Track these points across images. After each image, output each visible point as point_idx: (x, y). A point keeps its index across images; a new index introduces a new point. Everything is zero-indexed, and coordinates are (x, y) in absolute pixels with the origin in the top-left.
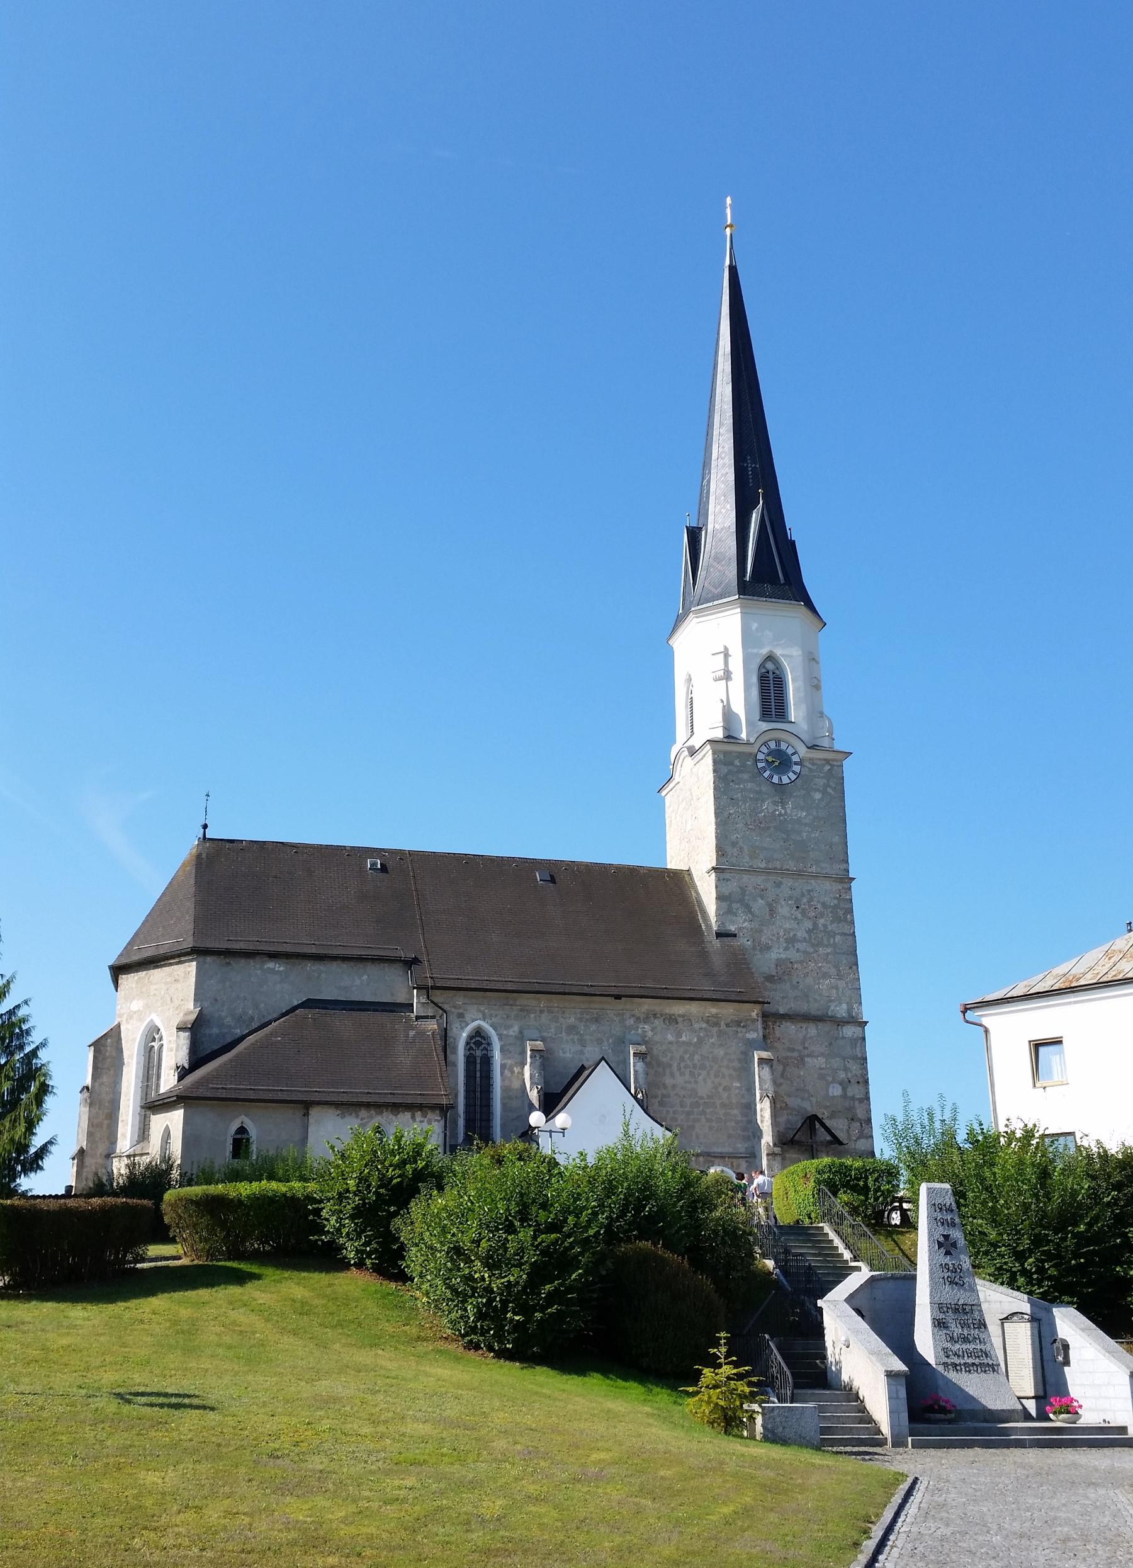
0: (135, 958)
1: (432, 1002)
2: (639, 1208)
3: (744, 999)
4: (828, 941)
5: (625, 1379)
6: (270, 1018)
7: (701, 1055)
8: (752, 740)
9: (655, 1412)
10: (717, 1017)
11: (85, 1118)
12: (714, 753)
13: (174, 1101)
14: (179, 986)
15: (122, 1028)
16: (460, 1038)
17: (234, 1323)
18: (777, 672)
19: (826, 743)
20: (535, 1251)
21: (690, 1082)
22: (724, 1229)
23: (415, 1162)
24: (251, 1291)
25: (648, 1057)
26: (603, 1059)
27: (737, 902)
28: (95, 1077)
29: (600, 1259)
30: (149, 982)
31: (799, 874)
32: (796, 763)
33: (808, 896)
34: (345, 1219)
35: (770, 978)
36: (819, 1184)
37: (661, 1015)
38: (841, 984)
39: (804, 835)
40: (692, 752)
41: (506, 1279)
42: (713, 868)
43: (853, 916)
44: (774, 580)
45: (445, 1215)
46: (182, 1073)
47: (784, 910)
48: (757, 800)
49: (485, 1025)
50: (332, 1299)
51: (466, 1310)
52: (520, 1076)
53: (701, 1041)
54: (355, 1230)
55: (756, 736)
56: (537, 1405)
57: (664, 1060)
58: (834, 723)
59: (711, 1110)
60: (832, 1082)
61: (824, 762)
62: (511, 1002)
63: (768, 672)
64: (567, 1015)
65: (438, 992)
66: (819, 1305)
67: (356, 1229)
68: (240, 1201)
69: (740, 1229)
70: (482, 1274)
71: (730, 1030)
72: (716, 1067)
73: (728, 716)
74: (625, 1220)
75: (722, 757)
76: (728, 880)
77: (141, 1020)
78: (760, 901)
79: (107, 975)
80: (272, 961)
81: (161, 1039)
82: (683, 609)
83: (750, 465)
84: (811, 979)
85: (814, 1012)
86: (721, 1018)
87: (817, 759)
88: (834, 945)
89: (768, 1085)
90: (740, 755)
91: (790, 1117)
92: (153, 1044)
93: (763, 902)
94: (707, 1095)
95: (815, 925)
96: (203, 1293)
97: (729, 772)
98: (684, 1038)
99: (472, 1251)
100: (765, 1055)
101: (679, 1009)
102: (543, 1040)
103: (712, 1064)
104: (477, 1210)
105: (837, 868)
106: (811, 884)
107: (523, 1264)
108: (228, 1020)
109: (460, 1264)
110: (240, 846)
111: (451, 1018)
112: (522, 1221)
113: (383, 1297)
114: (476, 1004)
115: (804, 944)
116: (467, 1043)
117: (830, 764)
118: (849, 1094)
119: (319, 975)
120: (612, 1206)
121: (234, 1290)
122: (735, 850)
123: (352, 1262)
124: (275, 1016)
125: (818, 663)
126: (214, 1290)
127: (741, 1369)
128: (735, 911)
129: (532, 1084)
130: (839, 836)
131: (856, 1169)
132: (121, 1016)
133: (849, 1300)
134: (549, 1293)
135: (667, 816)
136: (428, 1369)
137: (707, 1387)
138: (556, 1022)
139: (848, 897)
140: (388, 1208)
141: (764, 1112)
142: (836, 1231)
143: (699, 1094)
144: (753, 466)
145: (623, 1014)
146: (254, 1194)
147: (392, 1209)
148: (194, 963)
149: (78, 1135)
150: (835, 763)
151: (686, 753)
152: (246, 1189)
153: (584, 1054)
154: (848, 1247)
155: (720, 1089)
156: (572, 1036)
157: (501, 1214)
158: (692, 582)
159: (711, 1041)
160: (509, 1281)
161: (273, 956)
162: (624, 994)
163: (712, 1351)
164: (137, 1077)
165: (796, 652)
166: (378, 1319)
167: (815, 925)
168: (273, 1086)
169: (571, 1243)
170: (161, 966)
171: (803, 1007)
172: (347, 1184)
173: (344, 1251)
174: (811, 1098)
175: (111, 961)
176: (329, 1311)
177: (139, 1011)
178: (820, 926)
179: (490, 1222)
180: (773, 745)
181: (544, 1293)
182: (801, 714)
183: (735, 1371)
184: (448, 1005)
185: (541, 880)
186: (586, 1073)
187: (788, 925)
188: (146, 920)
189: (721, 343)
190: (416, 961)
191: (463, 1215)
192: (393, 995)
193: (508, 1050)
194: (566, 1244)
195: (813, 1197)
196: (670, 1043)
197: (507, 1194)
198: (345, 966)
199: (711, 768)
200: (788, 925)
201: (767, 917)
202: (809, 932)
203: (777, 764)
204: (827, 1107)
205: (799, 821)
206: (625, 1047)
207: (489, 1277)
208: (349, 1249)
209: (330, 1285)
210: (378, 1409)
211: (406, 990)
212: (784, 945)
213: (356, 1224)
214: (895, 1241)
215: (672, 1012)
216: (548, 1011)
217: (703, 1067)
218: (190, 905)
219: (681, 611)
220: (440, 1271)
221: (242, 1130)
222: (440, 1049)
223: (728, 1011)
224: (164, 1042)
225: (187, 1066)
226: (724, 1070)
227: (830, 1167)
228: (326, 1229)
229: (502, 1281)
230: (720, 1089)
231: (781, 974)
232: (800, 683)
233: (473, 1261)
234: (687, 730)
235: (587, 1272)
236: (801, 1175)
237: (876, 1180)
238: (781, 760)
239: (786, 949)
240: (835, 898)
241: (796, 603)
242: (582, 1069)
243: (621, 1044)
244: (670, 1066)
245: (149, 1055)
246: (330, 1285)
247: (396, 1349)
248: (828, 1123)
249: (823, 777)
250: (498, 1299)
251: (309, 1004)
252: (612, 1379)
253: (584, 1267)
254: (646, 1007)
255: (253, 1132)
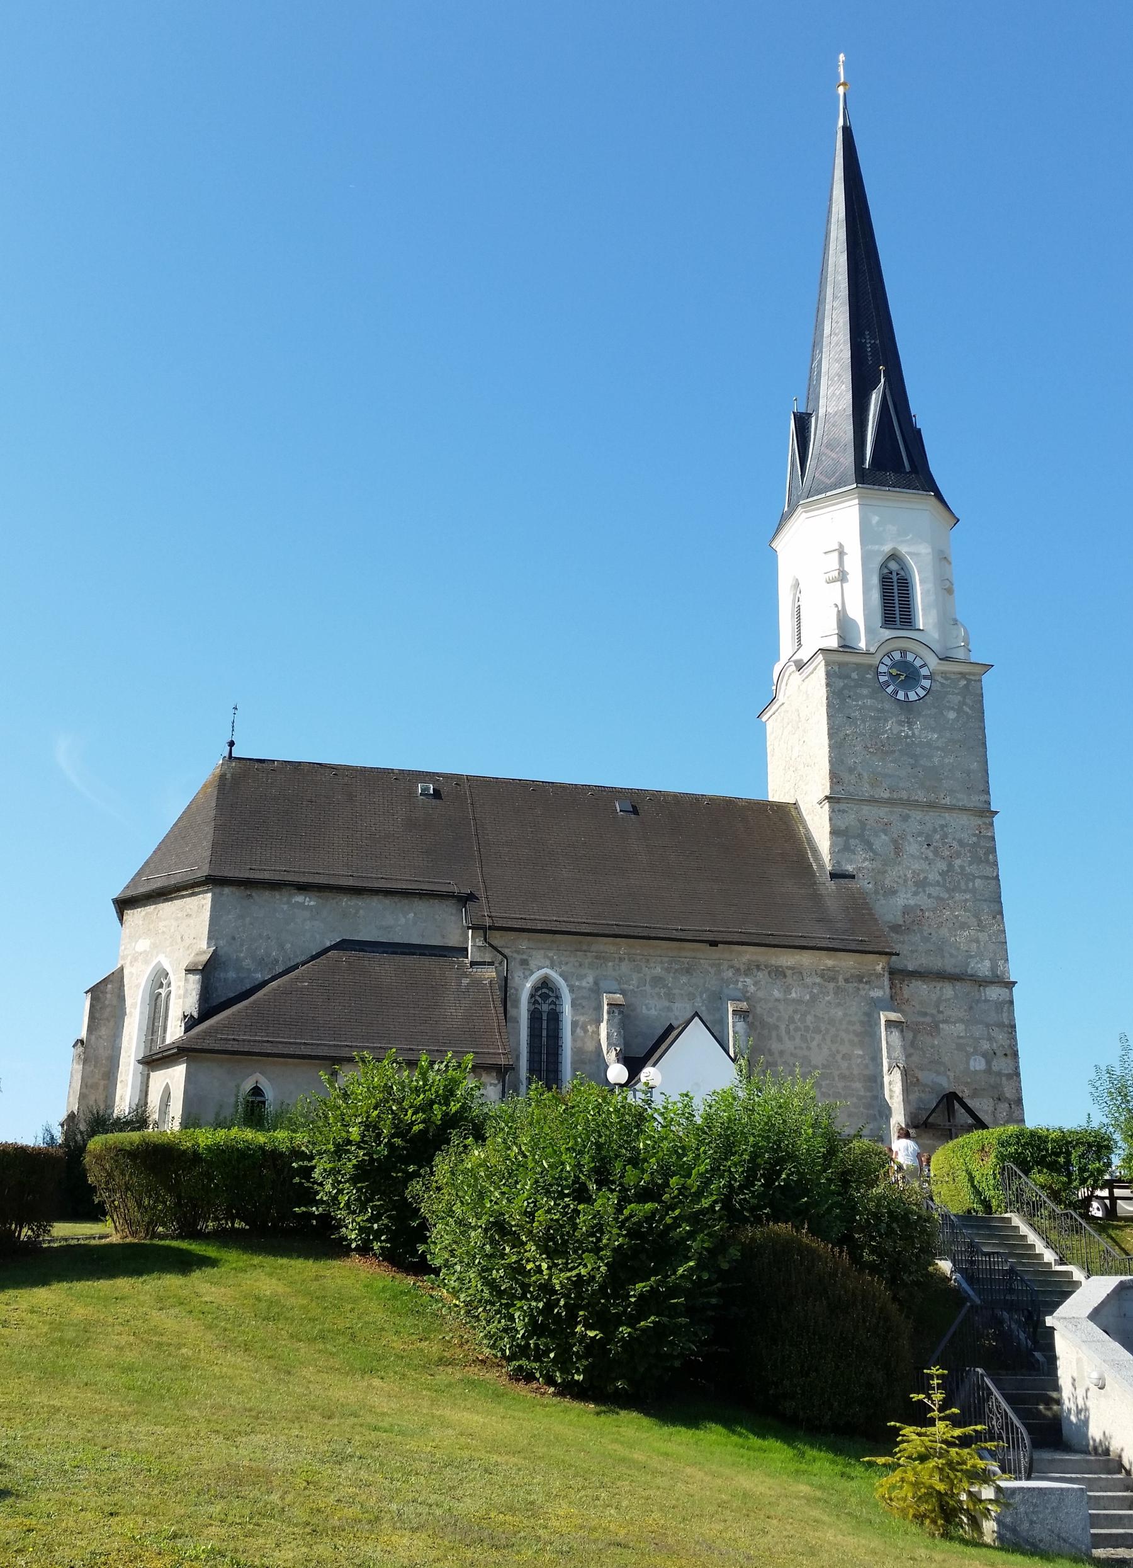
0: (142, 890)
1: (491, 945)
2: (772, 1175)
3: (867, 949)
4: (967, 884)
5: (762, 1435)
6: (298, 960)
7: (815, 1016)
8: (872, 650)
9: (818, 1494)
10: (833, 971)
11: (78, 1077)
12: (827, 665)
13: (173, 1055)
14: (191, 921)
15: (126, 972)
16: (523, 989)
17: (154, 1331)
18: (902, 573)
19: (960, 654)
20: (620, 1228)
21: (801, 1048)
22: (890, 1212)
23: (447, 1104)
24: (197, 1282)
25: (751, 1016)
26: (696, 1014)
27: (854, 837)
28: (91, 1029)
29: (720, 1246)
30: (157, 918)
31: (931, 806)
32: (925, 677)
33: (941, 833)
34: (345, 1182)
35: (896, 928)
36: (1003, 1160)
37: (766, 967)
38: (984, 937)
39: (936, 760)
40: (800, 666)
41: (574, 1273)
42: (827, 798)
43: (996, 856)
44: (898, 468)
45: (483, 1174)
46: (190, 1023)
47: (912, 847)
48: (879, 719)
49: (554, 975)
50: (317, 1298)
51: (511, 1318)
52: (595, 1036)
53: (814, 998)
54: (358, 1199)
55: (877, 645)
56: (625, 1485)
57: (770, 1020)
58: (968, 629)
59: (828, 1082)
60: (973, 1054)
61: (959, 676)
62: (585, 948)
63: (891, 573)
64: (652, 965)
65: (497, 934)
66: (1048, 1324)
67: (359, 1197)
68: (196, 1154)
69: (912, 1212)
70: (537, 1264)
71: (850, 987)
72: (833, 1031)
73: (844, 624)
74: (752, 1192)
75: (836, 668)
76: (844, 811)
77: (147, 962)
78: (883, 837)
79: (112, 910)
80: (301, 894)
81: (169, 985)
82: (788, 506)
83: (868, 341)
84: (946, 930)
85: (950, 969)
86: (838, 971)
87: (951, 673)
88: (974, 891)
89: (898, 1053)
90: (858, 666)
91: (923, 1095)
92: (160, 990)
93: (886, 838)
94: (822, 1064)
95: (950, 866)
96: (123, 1284)
97: (845, 687)
98: (794, 995)
99: (522, 1227)
100: (894, 1016)
101: (787, 959)
102: (623, 992)
103: (828, 1027)
104: (531, 1165)
105: (975, 800)
106: (945, 818)
107: (602, 1249)
108: (248, 963)
109: (504, 1249)
110: (271, 766)
111: (512, 964)
112: (600, 1184)
113: (395, 1297)
114: (543, 949)
115: (937, 888)
116: (532, 996)
117: (967, 679)
118: (995, 1068)
119: (357, 912)
120: (732, 1170)
121: (172, 1281)
122: (853, 776)
123: (354, 1245)
124: (303, 958)
125: (950, 563)
126: (141, 1280)
127: (969, 1430)
128: (852, 848)
129: (609, 1045)
130: (976, 761)
131: (1053, 1141)
132: (124, 958)
133: (1095, 1315)
134: (641, 1297)
135: (768, 743)
136: (447, 1412)
137: (909, 1457)
138: (639, 972)
139: (989, 834)
140: (406, 1167)
141: (893, 1087)
142: (1031, 1225)
143: (813, 1062)
144: (873, 342)
145: (720, 965)
146: (218, 1145)
147: (411, 1168)
148: (209, 895)
149: (69, 1097)
150: (973, 678)
151: (793, 668)
152: (207, 1138)
153: (672, 1011)
154: (1049, 1244)
155: (839, 1057)
156: (657, 989)
157: (569, 1172)
158: (800, 473)
159: (827, 998)
160: (579, 1275)
161: (303, 888)
162: (721, 939)
163: (916, 1397)
164: (140, 1029)
165: (924, 549)
166: (383, 1329)
167: (950, 866)
168: (296, 1039)
169: (675, 1218)
170: (172, 899)
171: (936, 963)
172: (348, 1132)
173: (344, 1229)
174: (948, 1073)
175: (116, 893)
176: (309, 1315)
177: (145, 951)
178: (957, 867)
179: (551, 1185)
180: (897, 656)
181: (634, 1296)
182: (931, 621)
183: (958, 1432)
184: (509, 950)
185: (621, 811)
186: (675, 1032)
187: (916, 866)
188: (159, 848)
189: (834, 210)
190: (471, 897)
191: (511, 1175)
192: (443, 937)
193: (580, 1004)
194: (668, 1220)
195: (995, 1178)
196: (777, 1000)
197: (576, 1143)
198: (387, 901)
199: (824, 682)
200: (916, 866)
201: (892, 855)
202: (942, 874)
203: (903, 677)
204: (968, 1083)
205: (929, 744)
206: (722, 1004)
207: (549, 1268)
208: (350, 1227)
209: (317, 1278)
210: (332, 1499)
211: (460, 931)
212: (913, 890)
213: (359, 1190)
214: (1112, 1238)
215: (779, 963)
216: (629, 960)
217: (817, 1030)
218: (208, 831)
219: (786, 509)
220: (474, 1257)
221: (257, 1091)
222: (499, 1004)
223: (847, 963)
224: (172, 988)
225: (196, 1015)
226: (843, 1035)
227: (1018, 1137)
228: (318, 1198)
229: (569, 1274)
230: (839, 1057)
231: (911, 921)
232: (930, 586)
233: (523, 1244)
234: (793, 644)
235: (700, 1266)
236: (976, 1147)
237: (1082, 1156)
238: (907, 674)
239: (915, 894)
240: (975, 835)
241: (925, 493)
242: (670, 1028)
243: (717, 999)
244: (777, 1027)
245: (156, 1004)
246: (317, 1278)
247: (404, 1376)
248: (970, 1103)
249: (957, 694)
250: (562, 1303)
251: (344, 945)
252: (740, 1435)
253: (697, 1256)
254: (748, 957)
255: (270, 1094)
